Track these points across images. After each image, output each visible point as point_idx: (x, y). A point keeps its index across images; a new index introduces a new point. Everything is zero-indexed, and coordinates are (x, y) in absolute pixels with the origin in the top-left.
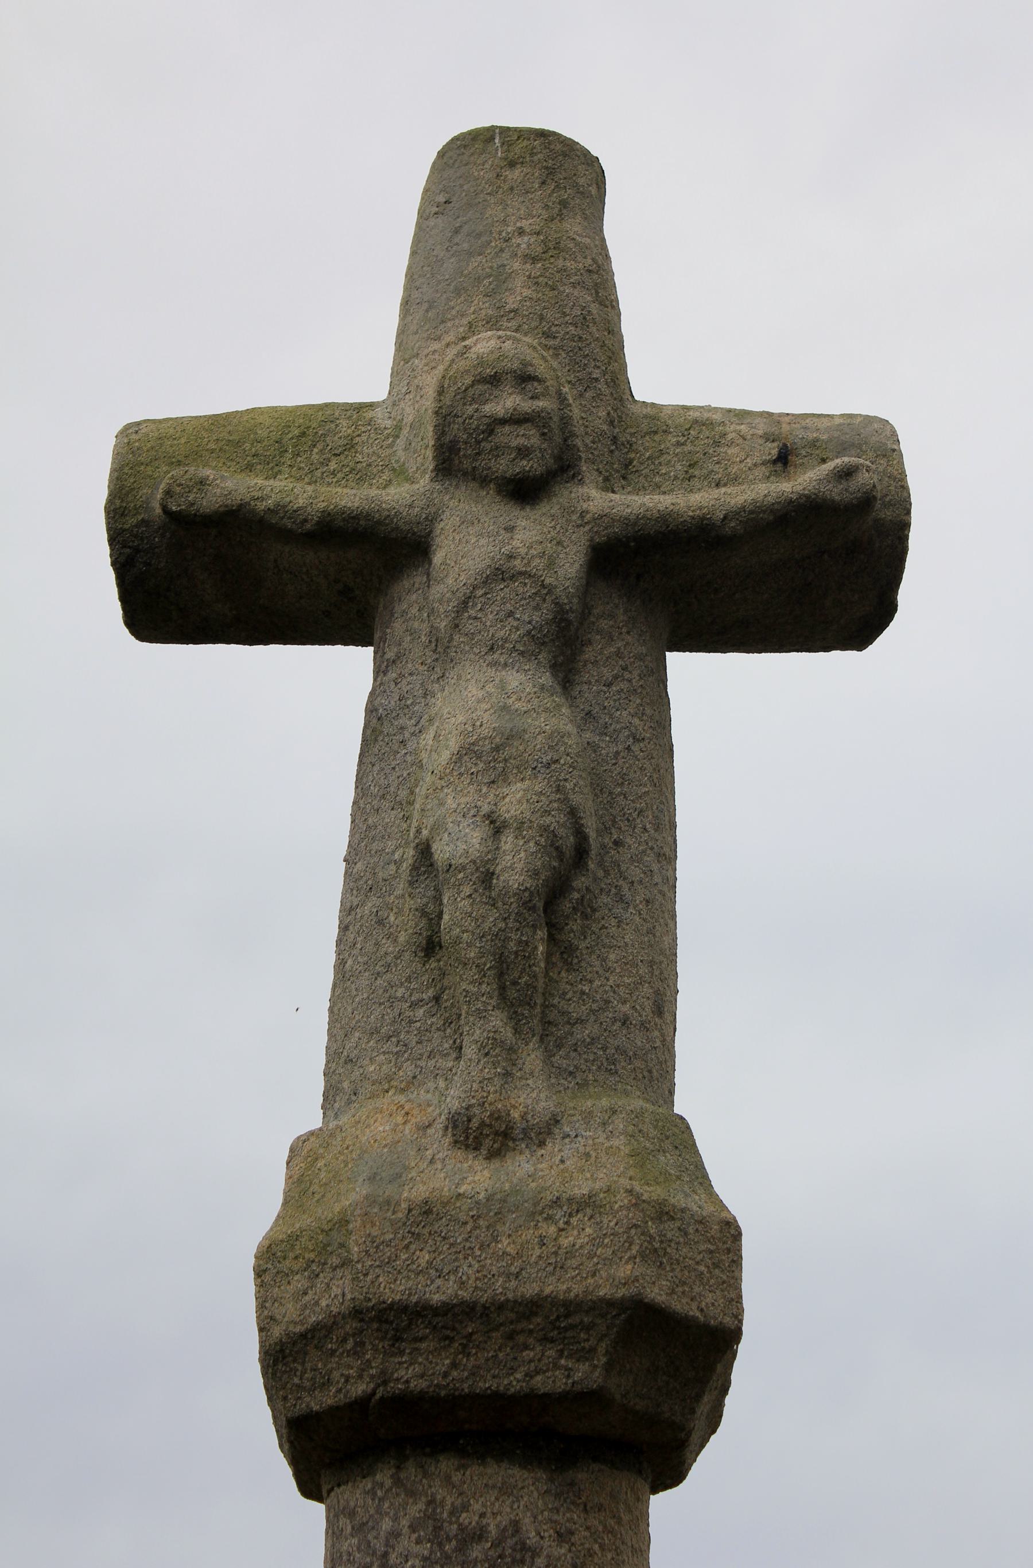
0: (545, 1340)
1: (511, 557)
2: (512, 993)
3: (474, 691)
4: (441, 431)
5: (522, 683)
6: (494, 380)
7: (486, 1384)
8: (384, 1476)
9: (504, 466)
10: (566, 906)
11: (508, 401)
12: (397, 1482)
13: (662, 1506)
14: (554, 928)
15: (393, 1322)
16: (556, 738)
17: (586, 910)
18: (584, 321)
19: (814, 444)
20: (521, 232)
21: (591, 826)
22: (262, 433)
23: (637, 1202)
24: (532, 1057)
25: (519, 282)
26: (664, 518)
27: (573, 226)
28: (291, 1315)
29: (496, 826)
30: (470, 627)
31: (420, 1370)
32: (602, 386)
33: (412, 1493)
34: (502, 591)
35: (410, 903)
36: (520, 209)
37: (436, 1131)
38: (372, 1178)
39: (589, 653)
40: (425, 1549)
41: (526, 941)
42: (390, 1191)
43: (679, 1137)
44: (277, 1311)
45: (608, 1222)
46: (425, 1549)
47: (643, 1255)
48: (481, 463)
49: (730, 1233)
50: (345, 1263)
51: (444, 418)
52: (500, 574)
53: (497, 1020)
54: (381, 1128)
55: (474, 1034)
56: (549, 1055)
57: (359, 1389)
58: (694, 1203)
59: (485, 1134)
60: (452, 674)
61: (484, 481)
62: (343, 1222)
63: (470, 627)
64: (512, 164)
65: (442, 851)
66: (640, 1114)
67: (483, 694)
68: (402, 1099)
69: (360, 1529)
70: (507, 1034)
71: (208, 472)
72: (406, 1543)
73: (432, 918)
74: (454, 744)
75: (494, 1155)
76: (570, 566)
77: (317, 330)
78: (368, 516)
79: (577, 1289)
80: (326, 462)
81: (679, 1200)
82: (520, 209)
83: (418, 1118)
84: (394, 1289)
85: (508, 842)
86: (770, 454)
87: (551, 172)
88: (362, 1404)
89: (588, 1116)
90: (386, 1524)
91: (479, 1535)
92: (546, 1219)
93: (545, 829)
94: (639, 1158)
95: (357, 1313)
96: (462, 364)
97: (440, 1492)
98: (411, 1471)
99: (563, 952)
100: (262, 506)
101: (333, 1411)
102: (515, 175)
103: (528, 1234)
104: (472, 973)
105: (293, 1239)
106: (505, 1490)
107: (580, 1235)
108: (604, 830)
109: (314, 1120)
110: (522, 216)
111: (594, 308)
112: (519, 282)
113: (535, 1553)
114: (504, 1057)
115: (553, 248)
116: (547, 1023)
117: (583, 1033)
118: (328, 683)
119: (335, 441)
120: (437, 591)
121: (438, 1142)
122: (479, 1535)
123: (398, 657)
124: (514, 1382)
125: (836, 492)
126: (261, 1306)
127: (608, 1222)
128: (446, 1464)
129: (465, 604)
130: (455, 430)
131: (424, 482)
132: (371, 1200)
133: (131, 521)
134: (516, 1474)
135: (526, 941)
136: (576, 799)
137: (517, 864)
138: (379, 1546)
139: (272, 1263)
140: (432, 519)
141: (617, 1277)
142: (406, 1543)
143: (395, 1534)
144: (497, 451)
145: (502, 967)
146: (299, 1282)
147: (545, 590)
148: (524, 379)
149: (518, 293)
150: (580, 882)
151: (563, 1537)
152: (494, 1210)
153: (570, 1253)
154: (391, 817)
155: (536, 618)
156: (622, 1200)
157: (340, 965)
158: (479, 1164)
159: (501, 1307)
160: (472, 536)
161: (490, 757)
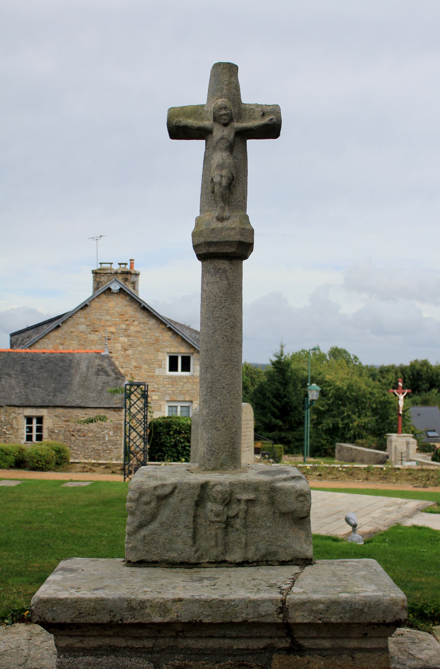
0: (228, 246)
1: (224, 136)
2: (224, 200)
3: (219, 156)
4: (214, 115)
5: (225, 154)
6: (221, 109)
7: (221, 251)
8: (209, 261)
9: (222, 121)
10: (231, 186)
11: (223, 112)
12: (210, 262)
13: (245, 262)
14: (230, 189)
15: (209, 244)
16: (230, 163)
17: (234, 186)
18: (234, 95)
19: (268, 112)
20: (225, 81)
21: (235, 176)
22: (188, 112)
23: (240, 228)
24: (227, 208)
25: (225, 90)
26: (245, 128)
27: (233, 79)
28: (197, 242)
29: (222, 176)
30: (218, 146)
31: (212, 250)
32: (237, 105)
33: (212, 264)
34: (222, 141)
35: (211, 186)
36: (225, 75)
37: (214, 218)
38: (206, 225)
39: (235, 148)
40: (214, 271)
41: (227, 190)
42: (208, 227)
43: (247, 217)
44: (194, 241)
45: (236, 231)
46: (214, 271)
47: (240, 235)
48: (219, 121)
49: (253, 230)
50: (203, 236)
51: (214, 114)
52: (222, 138)
53: (222, 204)
54: (207, 218)
55: (219, 206)
56: (229, 207)
57: (205, 252)
58: (247, 227)
59: (221, 219)
60: (216, 152)
61: (220, 123)
62: (202, 231)
63: (218, 146)
64: (224, 69)
65: (215, 180)
66: (241, 215)
67: (220, 157)
68: (210, 213)
69: (206, 268)
70: (224, 205)
71: (181, 120)
72: (211, 270)
73: (214, 189)
74: (216, 164)
75: (222, 222)
76: (232, 136)
77: (196, 93)
78: (204, 127)
79: (232, 240)
80: (198, 117)
81: (246, 227)
82: (225, 75)
83: (212, 216)
84: (209, 240)
85: (223, 179)
86: (241, 178)
87: (230, 70)
88: (206, 253)
89: (234, 216)
90: (209, 267)
91: (220, 269)
92: (229, 230)
93: (228, 177)
94: (240, 222)
95: (205, 243)
96: (216, 106)
97: (215, 264)
98: (212, 261)
99: (231, 193)
100: (189, 125)
101: (202, 254)
102: (224, 71)
103: (226, 233)
104: (219, 197)
105: (196, 232)
106: (224, 263)
107: (232, 233)
108: (237, 174)
109: (199, 215)
110: (225, 78)
111: (236, 93)
112: (225, 90)
113: (227, 271)
114: (223, 209)
115: (230, 83)
116: (229, 203)
117: (234, 204)
118: (199, 145)
119: (199, 113)
120: (214, 139)
121: (214, 219)
122: (220, 269)
123: (209, 148)
124: (224, 251)
125: (270, 123)
126: (192, 240)
127: (236, 231)
128: (216, 260)
129: (217, 143)
130: (216, 115)
131: (212, 122)
132: (206, 228)
133: (170, 126)
134: (224, 261)
135: (227, 190)
136: (232, 172)
137: (224, 182)
138: (208, 270)
139: (194, 235)
140: (213, 128)
141: (238, 238)
142: (211, 270)
143: (210, 269)
144: (222, 119)
145: (223, 196)
146: (197, 238)
147: (228, 140)
148: (225, 108)
149: (225, 92)
150: (233, 183)
151: (231, 269)
152: (222, 229)
153: (231, 235)
154: (208, 172)
155: (227, 145)
156: (238, 228)
157: (201, 192)
158: (220, 223)
159: (223, 242)
160: (219, 132)
161: (221, 166)
